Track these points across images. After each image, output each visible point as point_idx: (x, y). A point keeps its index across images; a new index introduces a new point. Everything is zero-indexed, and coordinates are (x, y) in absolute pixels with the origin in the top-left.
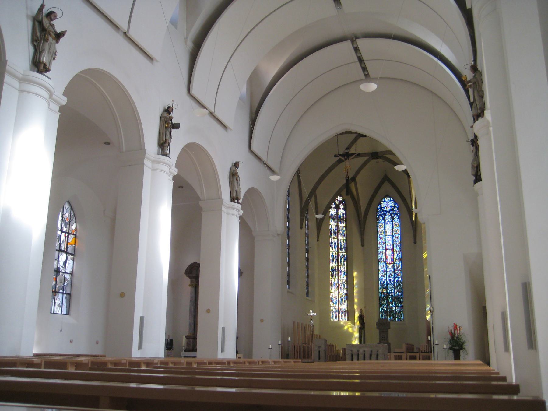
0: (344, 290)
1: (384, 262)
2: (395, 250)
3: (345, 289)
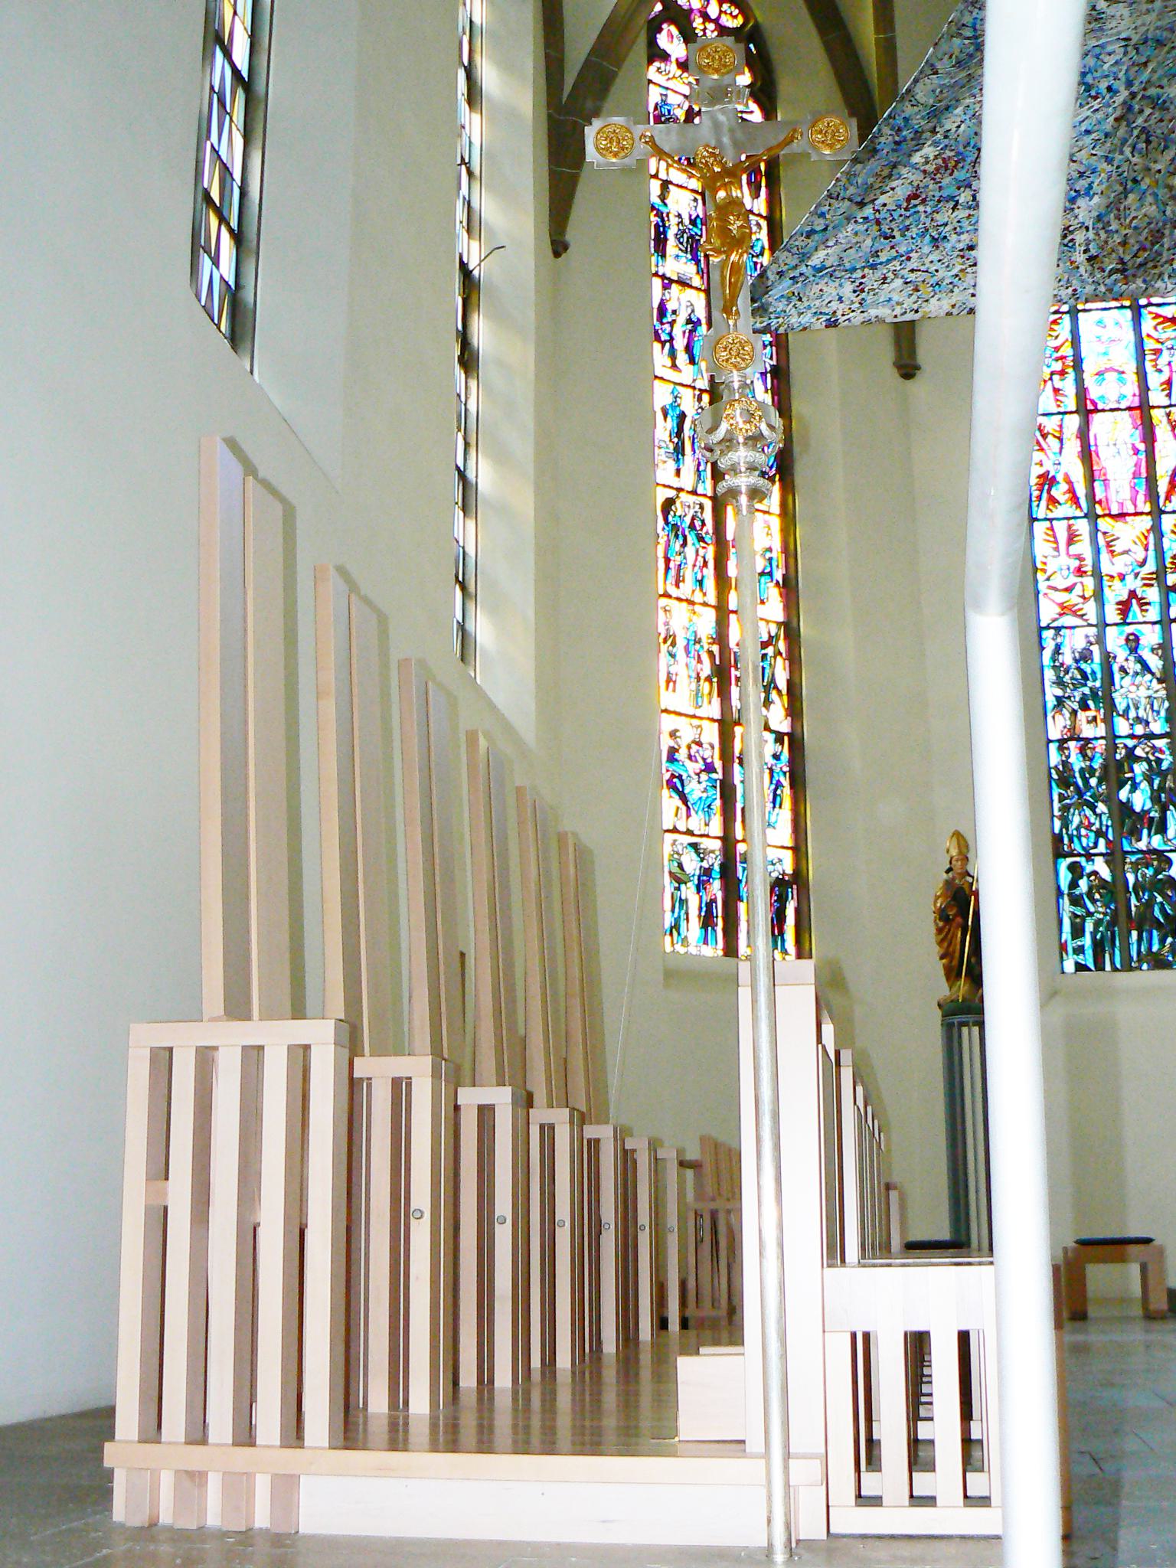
0: (767, 703)
1: (1078, 505)
2: (1157, 415)
3: (774, 695)
